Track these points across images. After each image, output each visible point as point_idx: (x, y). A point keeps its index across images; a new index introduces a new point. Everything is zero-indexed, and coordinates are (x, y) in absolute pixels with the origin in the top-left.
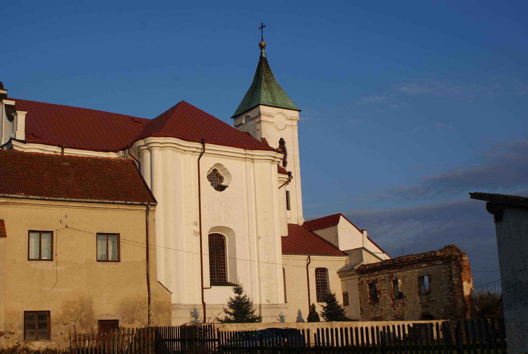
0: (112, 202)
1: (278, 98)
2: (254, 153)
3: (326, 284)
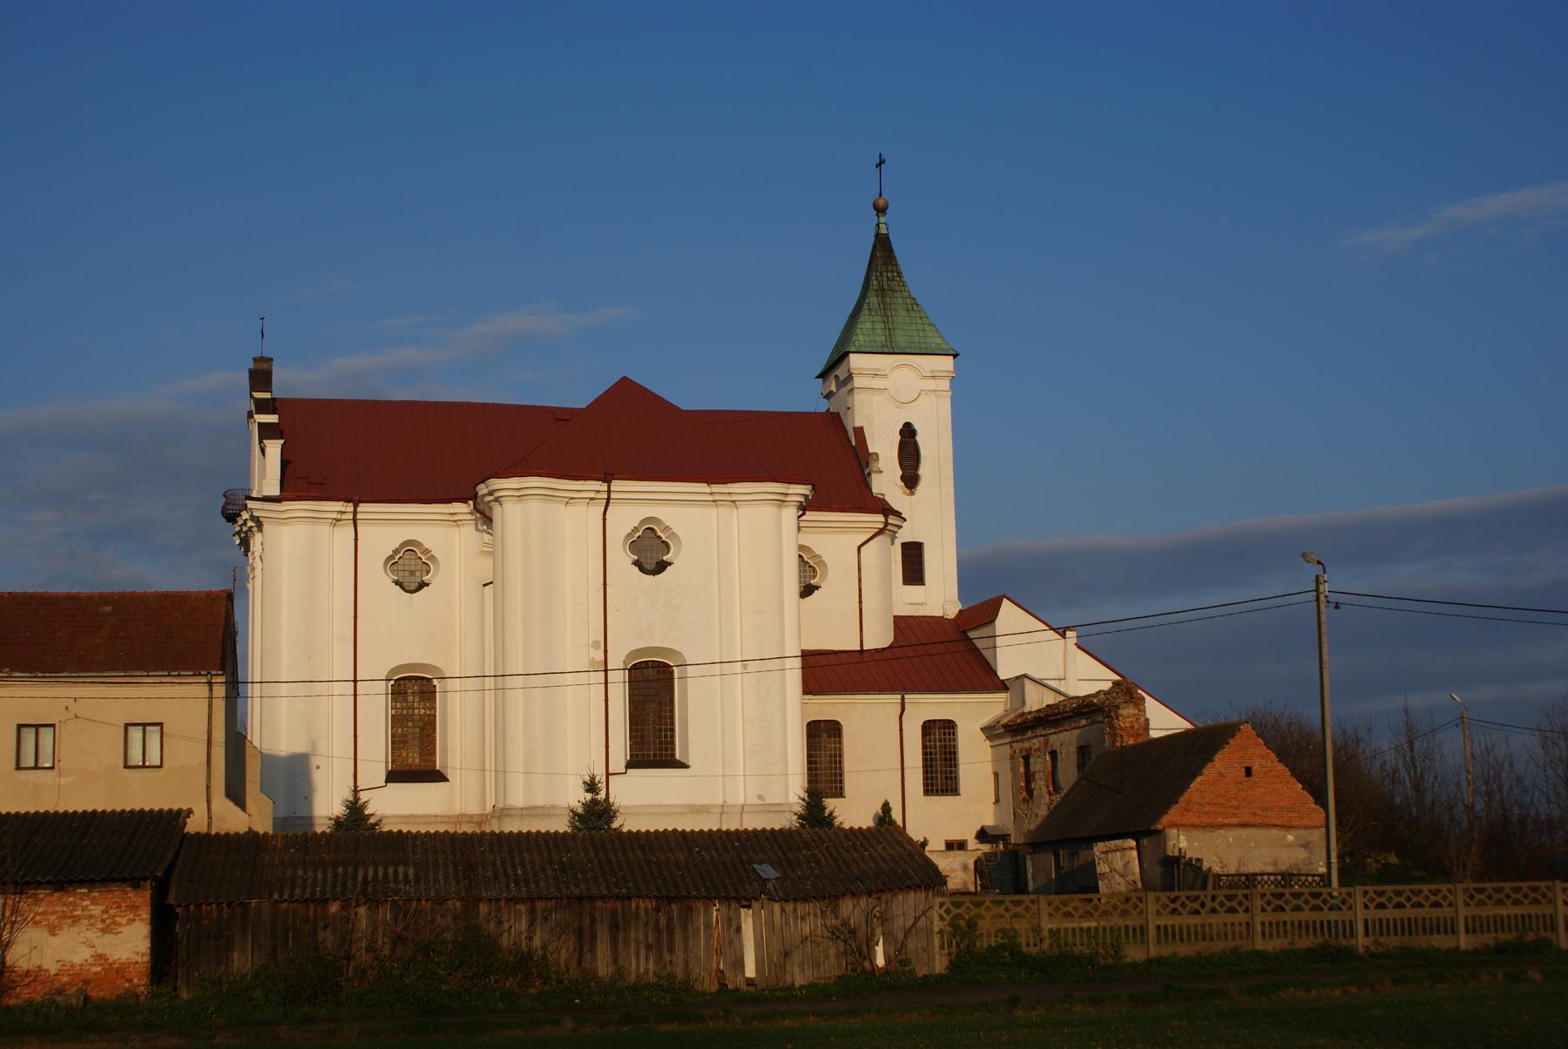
0: (146, 674)
1: (902, 330)
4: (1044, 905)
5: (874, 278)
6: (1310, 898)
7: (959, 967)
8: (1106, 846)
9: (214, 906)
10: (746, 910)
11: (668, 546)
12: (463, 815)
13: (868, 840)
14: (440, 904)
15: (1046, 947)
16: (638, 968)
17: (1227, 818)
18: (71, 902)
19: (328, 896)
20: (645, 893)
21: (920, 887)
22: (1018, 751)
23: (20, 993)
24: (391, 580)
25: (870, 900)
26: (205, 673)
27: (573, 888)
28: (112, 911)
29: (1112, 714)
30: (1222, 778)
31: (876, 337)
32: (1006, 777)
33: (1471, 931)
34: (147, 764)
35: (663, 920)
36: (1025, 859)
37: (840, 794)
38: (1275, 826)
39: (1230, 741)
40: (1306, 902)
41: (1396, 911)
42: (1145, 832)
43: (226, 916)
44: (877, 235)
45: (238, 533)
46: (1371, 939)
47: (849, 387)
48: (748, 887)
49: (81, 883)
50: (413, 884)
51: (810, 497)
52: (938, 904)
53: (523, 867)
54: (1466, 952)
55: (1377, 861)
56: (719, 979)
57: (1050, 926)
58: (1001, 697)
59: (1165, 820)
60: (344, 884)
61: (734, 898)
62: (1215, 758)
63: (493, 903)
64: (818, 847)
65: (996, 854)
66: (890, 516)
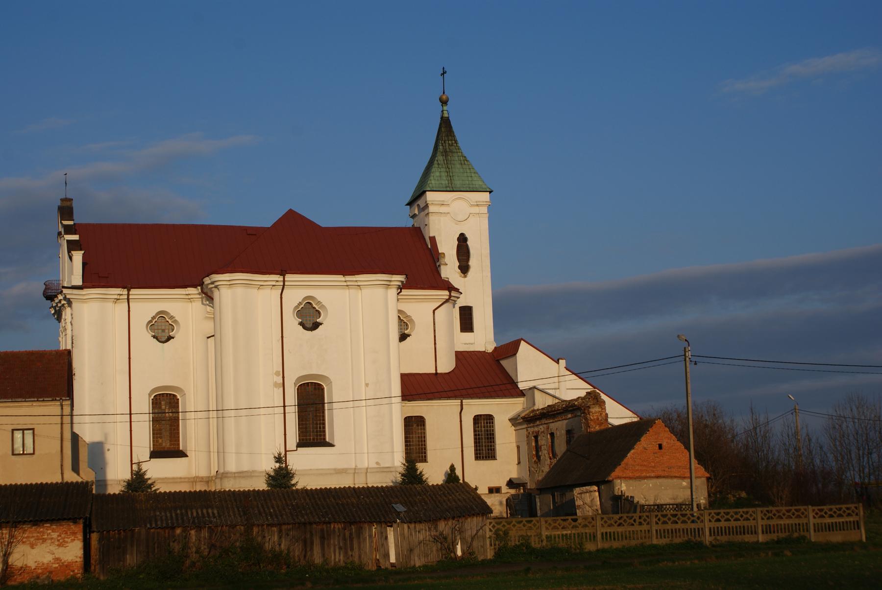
0: (24, 400)
1: (458, 176)
2: (357, 279)
3: (423, 446)
4: (543, 523)
5: (440, 144)
6: (681, 517)
7: (500, 555)
8: (580, 490)
9: (116, 531)
10: (390, 528)
11: (319, 313)
12: (197, 477)
13: (451, 491)
14: (233, 528)
15: (544, 544)
16: (335, 559)
17: (648, 473)
18: (42, 531)
19: (175, 525)
20: (338, 520)
21: (479, 514)
22: (531, 433)
23: (16, 579)
24: (151, 335)
25: (454, 521)
26: (59, 399)
27: (300, 518)
28: (63, 536)
29: (586, 411)
30: (645, 451)
31: (442, 181)
32: (524, 448)
33: (765, 532)
34: (25, 452)
35: (347, 534)
36: (535, 498)
37: (424, 460)
38: (676, 477)
39: (650, 429)
40: (669, 519)
41: (726, 523)
42: (602, 481)
43: (122, 537)
44: (442, 118)
45: (55, 308)
46: (713, 537)
47: (426, 212)
48: (390, 516)
49: (47, 521)
50: (218, 518)
51: (405, 282)
52: (488, 523)
53: (273, 508)
54: (762, 543)
55: (734, 496)
56: (376, 564)
57: (546, 533)
58: (521, 400)
59: (613, 475)
60: (182, 518)
61: (384, 522)
62: (641, 439)
63: (260, 527)
64: (425, 494)
65: (519, 495)
66: (452, 292)
